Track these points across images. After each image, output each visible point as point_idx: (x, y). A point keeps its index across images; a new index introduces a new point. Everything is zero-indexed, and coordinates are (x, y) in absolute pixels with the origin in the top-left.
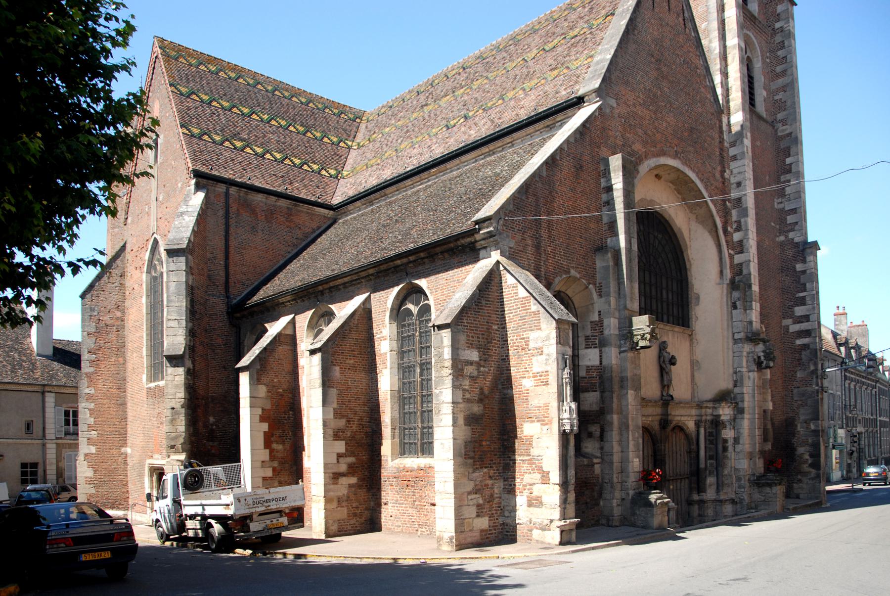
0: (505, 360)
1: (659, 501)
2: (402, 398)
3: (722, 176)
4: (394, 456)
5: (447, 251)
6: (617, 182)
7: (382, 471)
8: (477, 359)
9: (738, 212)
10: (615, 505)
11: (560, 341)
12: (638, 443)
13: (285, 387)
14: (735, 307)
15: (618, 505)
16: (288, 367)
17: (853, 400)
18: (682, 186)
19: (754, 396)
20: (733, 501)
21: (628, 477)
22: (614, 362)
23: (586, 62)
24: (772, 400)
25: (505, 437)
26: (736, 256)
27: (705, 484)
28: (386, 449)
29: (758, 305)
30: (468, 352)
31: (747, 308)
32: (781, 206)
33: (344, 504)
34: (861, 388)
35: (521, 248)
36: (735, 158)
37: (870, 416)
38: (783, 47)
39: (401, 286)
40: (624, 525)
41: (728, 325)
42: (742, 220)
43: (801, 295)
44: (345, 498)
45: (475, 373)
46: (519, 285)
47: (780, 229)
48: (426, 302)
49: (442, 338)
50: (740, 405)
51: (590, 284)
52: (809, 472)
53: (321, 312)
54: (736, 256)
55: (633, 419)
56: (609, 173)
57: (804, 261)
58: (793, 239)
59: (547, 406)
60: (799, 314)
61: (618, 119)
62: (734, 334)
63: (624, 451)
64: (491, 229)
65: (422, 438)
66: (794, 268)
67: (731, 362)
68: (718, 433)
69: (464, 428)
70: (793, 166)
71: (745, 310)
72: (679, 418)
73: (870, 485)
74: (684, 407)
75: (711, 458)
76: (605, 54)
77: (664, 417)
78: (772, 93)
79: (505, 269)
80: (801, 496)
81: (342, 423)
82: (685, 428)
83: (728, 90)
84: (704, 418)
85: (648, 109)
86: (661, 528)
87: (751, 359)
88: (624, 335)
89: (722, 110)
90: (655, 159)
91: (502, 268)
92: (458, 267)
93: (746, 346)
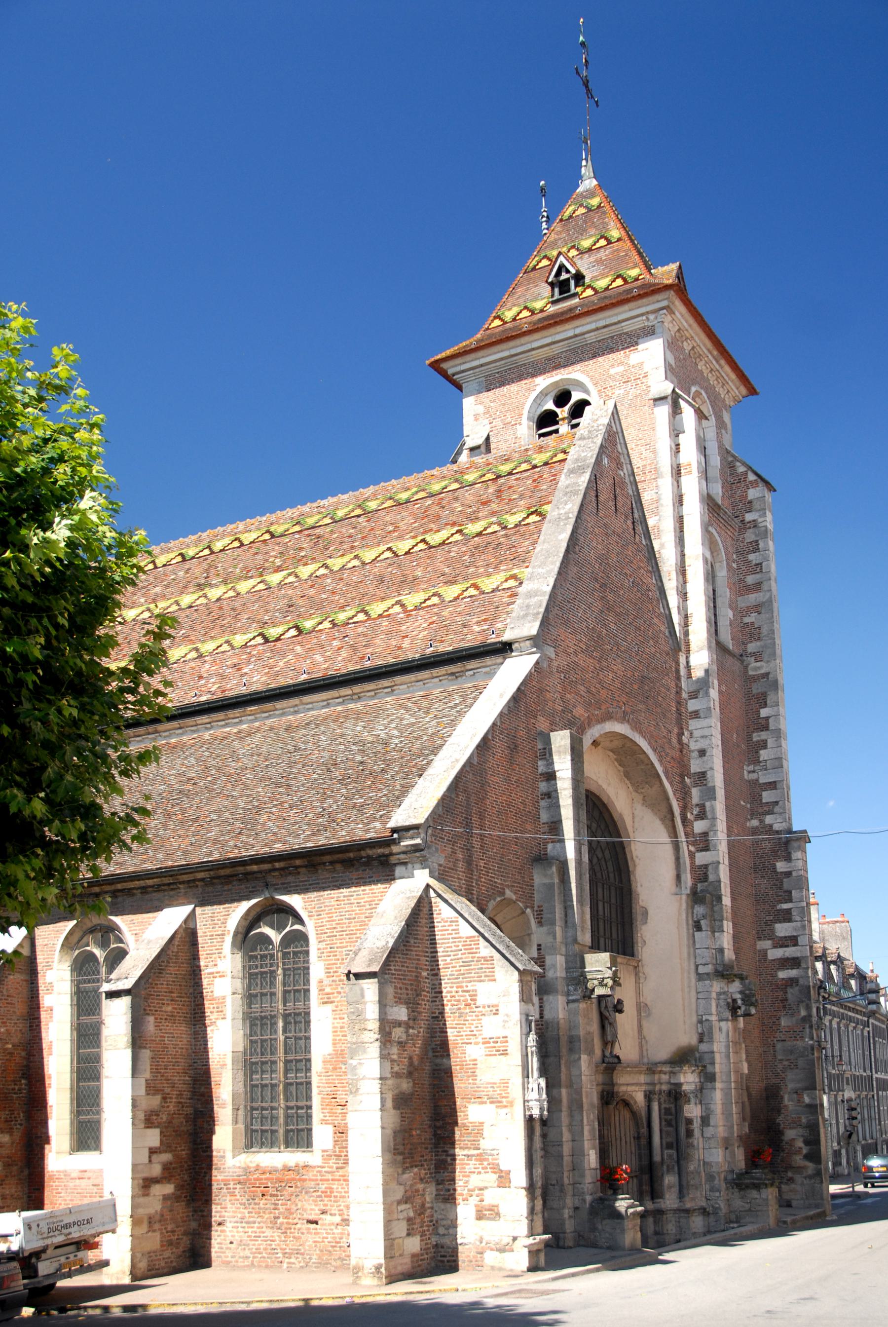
0: (438, 1020)
1: (631, 1211)
2: (254, 1060)
3: (680, 741)
4: (236, 1152)
5: (342, 862)
6: (563, 766)
7: (214, 1172)
8: (405, 1018)
9: (701, 791)
10: (566, 1216)
11: (525, 998)
12: (594, 1128)
13: (16, 1039)
14: (698, 927)
15: (570, 1217)
16: (20, 1008)
17: (836, 1047)
18: (625, 755)
19: (728, 1057)
20: (704, 1212)
21: (583, 1176)
22: (561, 1016)
23: (506, 585)
24: (747, 1060)
25: (438, 1124)
26: (698, 855)
27: (661, 1185)
28: (224, 1137)
29: (731, 924)
30: (396, 1009)
31: (716, 929)
32: (753, 776)
33: (157, 1226)
34: (847, 1026)
35: (450, 865)
36: (696, 715)
37: (861, 1072)
38: (756, 550)
39: (254, 901)
40: (579, 1246)
41: (689, 954)
42: (708, 804)
43: (785, 906)
44: (158, 1217)
45: (404, 1038)
46: (460, 919)
47: (752, 810)
48: (297, 927)
49: (362, 990)
50: (709, 1069)
51: (526, 907)
52: (804, 1168)
53: (89, 925)
54: (698, 855)
55: (587, 1096)
56: (551, 755)
57: (788, 858)
58: (771, 826)
59: (505, 1083)
60: (782, 934)
61: (557, 675)
62: (697, 969)
63: (577, 1138)
64: (418, 841)
65: (286, 1124)
66: (775, 868)
67: (694, 1006)
68: (679, 1110)
69: (393, 1112)
70: (771, 720)
71: (713, 932)
72: (623, 1088)
73: (873, 1186)
74: (630, 1073)
75: (669, 1146)
76: (539, 578)
77: (607, 1088)
78: (742, 613)
79: (439, 896)
80: (794, 1203)
81: (156, 1101)
82: (632, 1102)
83: (686, 617)
84: (657, 1088)
85: (591, 656)
86: (634, 1250)
87: (722, 1003)
88: (574, 979)
89: (678, 645)
90: (599, 727)
91: (432, 894)
92: (358, 885)
93: (715, 983)
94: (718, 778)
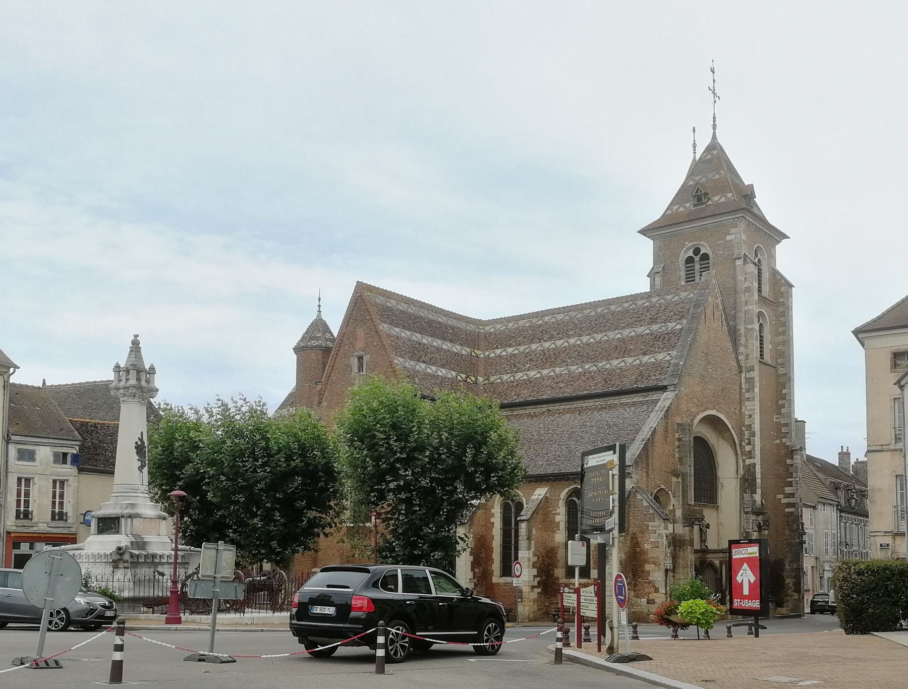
36: (748, 399)
38: (784, 316)
57: (792, 459)
94: (757, 427)
